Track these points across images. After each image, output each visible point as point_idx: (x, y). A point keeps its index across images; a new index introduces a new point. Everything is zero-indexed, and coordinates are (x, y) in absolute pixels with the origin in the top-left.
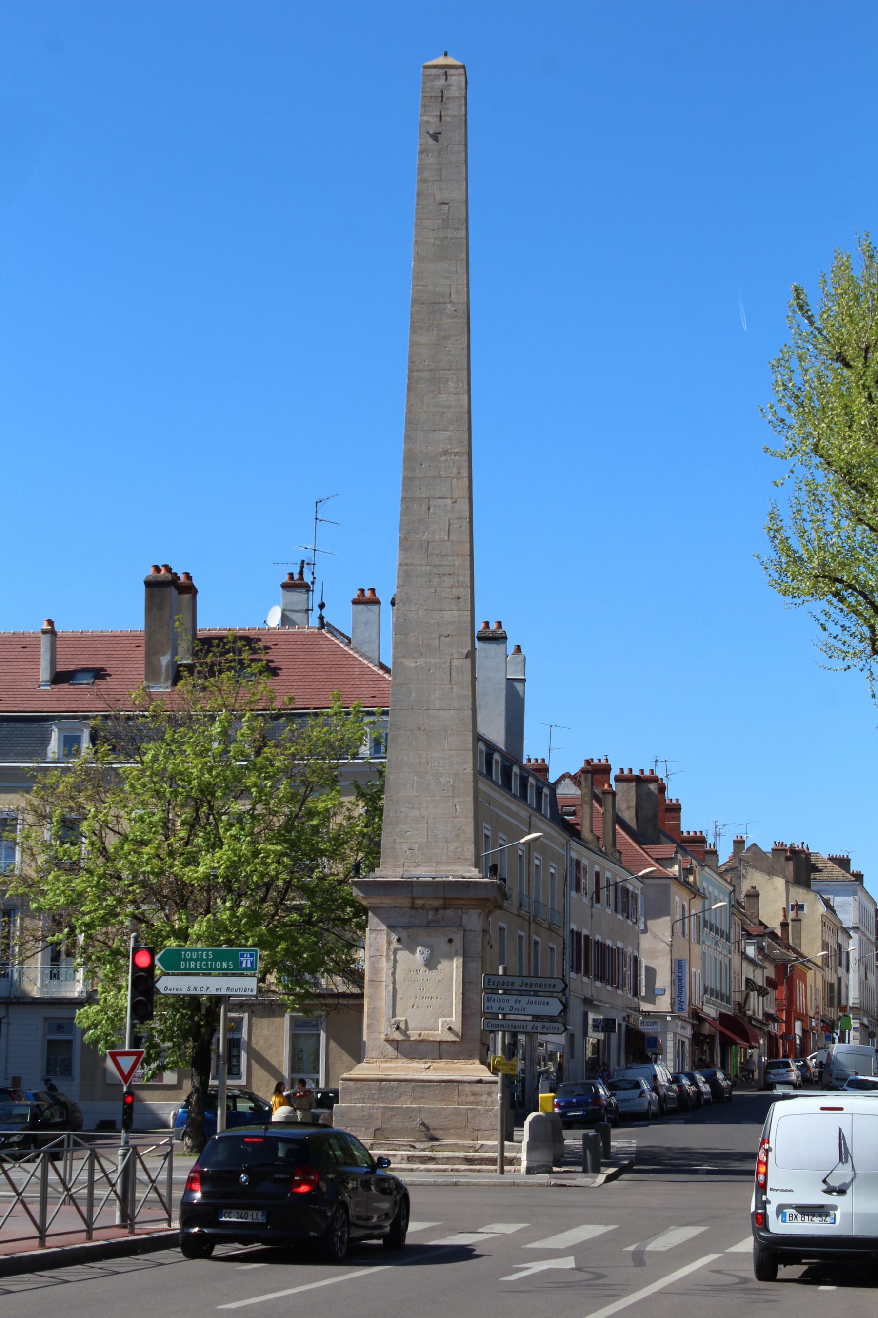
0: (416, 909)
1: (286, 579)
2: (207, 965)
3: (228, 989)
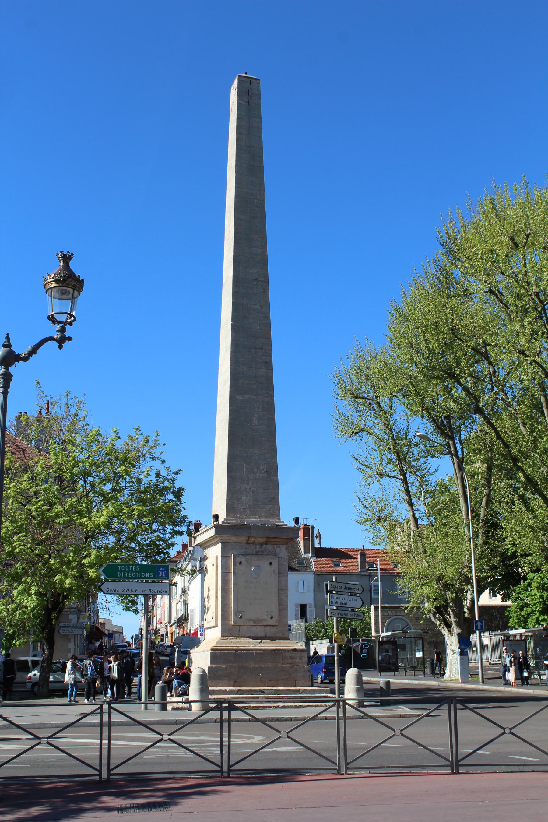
0: (249, 544)
2: (135, 575)
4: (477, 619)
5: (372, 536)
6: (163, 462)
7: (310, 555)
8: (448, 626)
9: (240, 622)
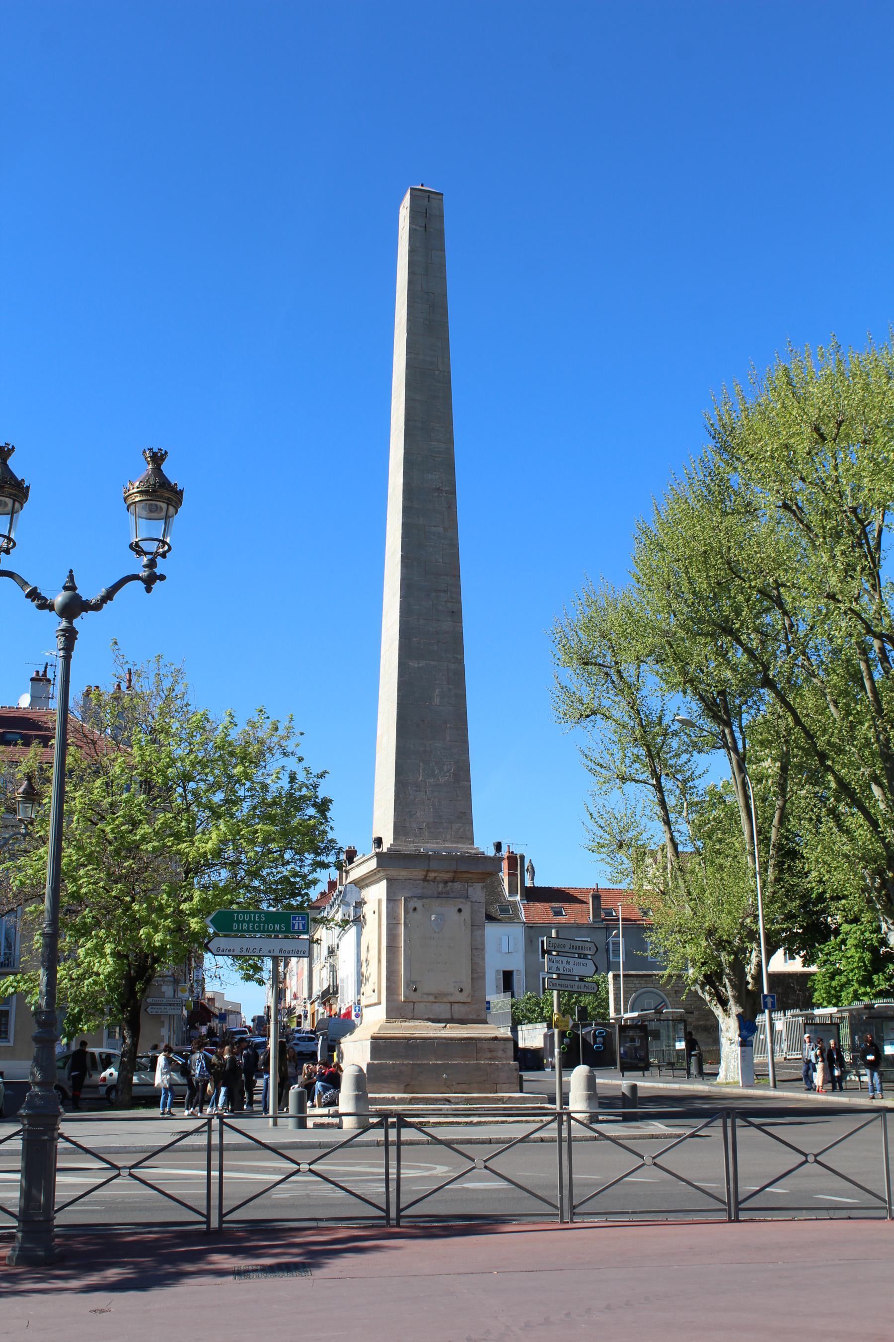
1: (34, 675)
2: (259, 927)
3: (281, 951)
4: (766, 992)
5: (610, 869)
6: (301, 760)
7: (518, 898)
8: (723, 1002)
9: (414, 997)
